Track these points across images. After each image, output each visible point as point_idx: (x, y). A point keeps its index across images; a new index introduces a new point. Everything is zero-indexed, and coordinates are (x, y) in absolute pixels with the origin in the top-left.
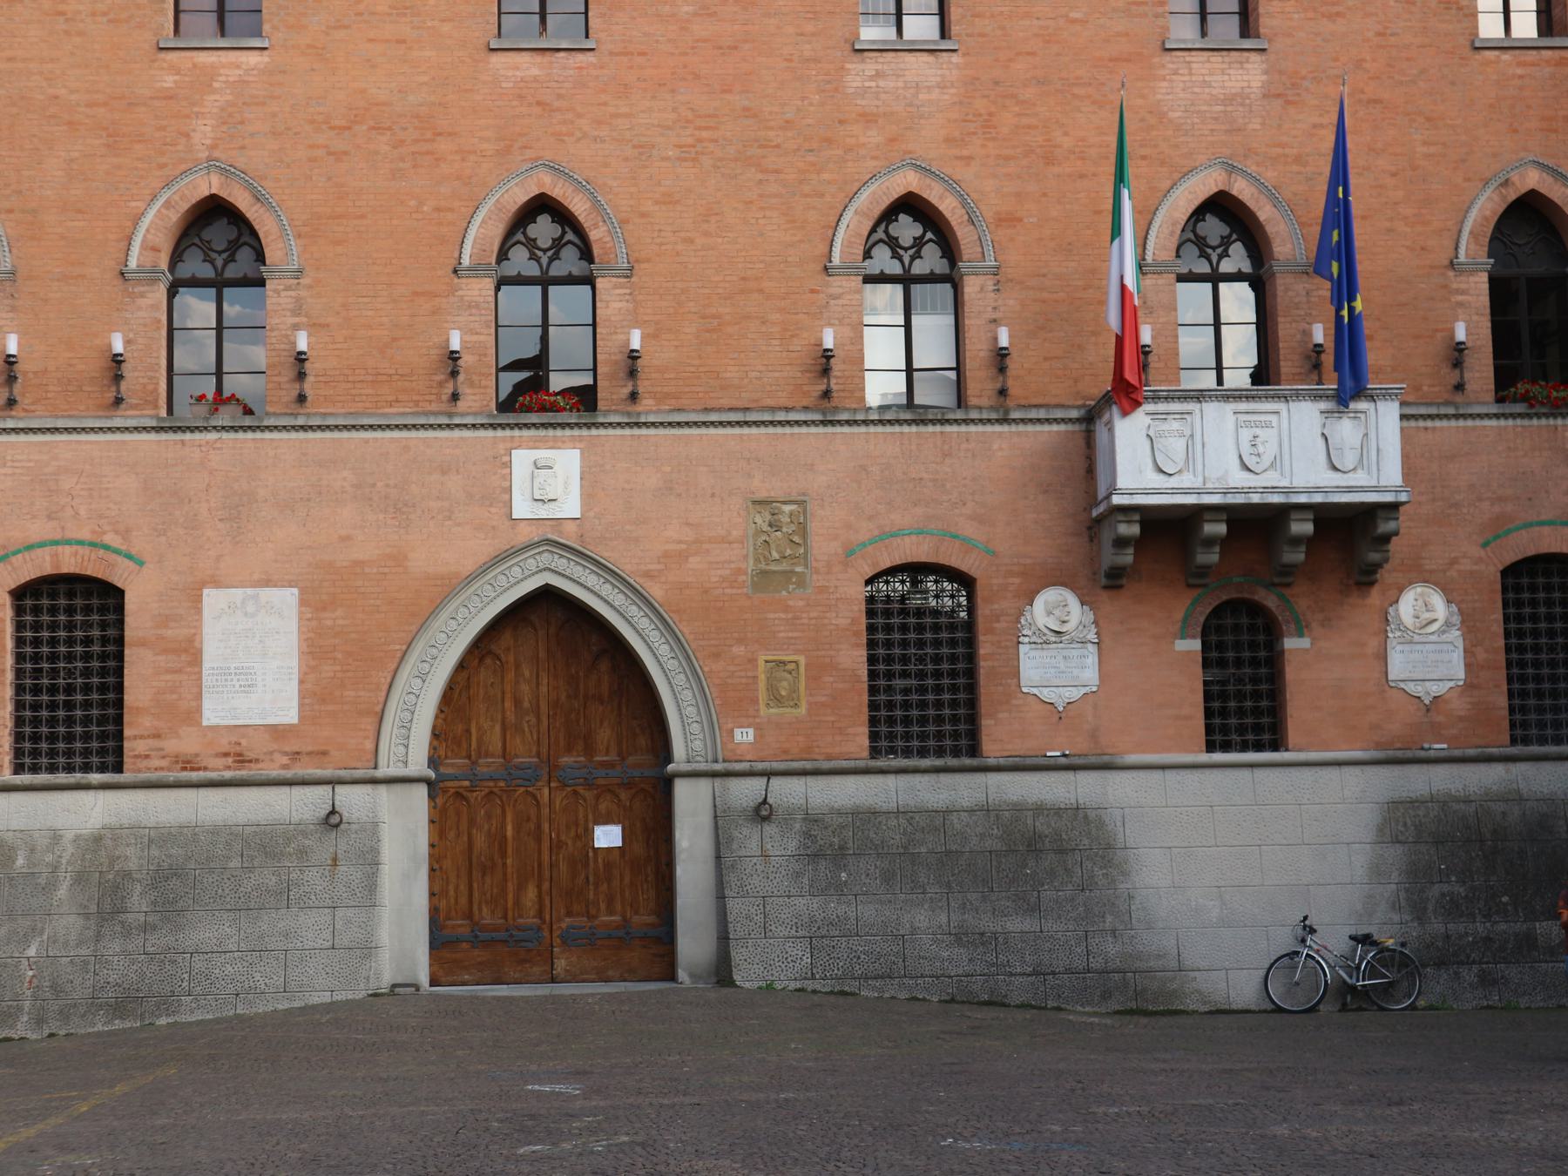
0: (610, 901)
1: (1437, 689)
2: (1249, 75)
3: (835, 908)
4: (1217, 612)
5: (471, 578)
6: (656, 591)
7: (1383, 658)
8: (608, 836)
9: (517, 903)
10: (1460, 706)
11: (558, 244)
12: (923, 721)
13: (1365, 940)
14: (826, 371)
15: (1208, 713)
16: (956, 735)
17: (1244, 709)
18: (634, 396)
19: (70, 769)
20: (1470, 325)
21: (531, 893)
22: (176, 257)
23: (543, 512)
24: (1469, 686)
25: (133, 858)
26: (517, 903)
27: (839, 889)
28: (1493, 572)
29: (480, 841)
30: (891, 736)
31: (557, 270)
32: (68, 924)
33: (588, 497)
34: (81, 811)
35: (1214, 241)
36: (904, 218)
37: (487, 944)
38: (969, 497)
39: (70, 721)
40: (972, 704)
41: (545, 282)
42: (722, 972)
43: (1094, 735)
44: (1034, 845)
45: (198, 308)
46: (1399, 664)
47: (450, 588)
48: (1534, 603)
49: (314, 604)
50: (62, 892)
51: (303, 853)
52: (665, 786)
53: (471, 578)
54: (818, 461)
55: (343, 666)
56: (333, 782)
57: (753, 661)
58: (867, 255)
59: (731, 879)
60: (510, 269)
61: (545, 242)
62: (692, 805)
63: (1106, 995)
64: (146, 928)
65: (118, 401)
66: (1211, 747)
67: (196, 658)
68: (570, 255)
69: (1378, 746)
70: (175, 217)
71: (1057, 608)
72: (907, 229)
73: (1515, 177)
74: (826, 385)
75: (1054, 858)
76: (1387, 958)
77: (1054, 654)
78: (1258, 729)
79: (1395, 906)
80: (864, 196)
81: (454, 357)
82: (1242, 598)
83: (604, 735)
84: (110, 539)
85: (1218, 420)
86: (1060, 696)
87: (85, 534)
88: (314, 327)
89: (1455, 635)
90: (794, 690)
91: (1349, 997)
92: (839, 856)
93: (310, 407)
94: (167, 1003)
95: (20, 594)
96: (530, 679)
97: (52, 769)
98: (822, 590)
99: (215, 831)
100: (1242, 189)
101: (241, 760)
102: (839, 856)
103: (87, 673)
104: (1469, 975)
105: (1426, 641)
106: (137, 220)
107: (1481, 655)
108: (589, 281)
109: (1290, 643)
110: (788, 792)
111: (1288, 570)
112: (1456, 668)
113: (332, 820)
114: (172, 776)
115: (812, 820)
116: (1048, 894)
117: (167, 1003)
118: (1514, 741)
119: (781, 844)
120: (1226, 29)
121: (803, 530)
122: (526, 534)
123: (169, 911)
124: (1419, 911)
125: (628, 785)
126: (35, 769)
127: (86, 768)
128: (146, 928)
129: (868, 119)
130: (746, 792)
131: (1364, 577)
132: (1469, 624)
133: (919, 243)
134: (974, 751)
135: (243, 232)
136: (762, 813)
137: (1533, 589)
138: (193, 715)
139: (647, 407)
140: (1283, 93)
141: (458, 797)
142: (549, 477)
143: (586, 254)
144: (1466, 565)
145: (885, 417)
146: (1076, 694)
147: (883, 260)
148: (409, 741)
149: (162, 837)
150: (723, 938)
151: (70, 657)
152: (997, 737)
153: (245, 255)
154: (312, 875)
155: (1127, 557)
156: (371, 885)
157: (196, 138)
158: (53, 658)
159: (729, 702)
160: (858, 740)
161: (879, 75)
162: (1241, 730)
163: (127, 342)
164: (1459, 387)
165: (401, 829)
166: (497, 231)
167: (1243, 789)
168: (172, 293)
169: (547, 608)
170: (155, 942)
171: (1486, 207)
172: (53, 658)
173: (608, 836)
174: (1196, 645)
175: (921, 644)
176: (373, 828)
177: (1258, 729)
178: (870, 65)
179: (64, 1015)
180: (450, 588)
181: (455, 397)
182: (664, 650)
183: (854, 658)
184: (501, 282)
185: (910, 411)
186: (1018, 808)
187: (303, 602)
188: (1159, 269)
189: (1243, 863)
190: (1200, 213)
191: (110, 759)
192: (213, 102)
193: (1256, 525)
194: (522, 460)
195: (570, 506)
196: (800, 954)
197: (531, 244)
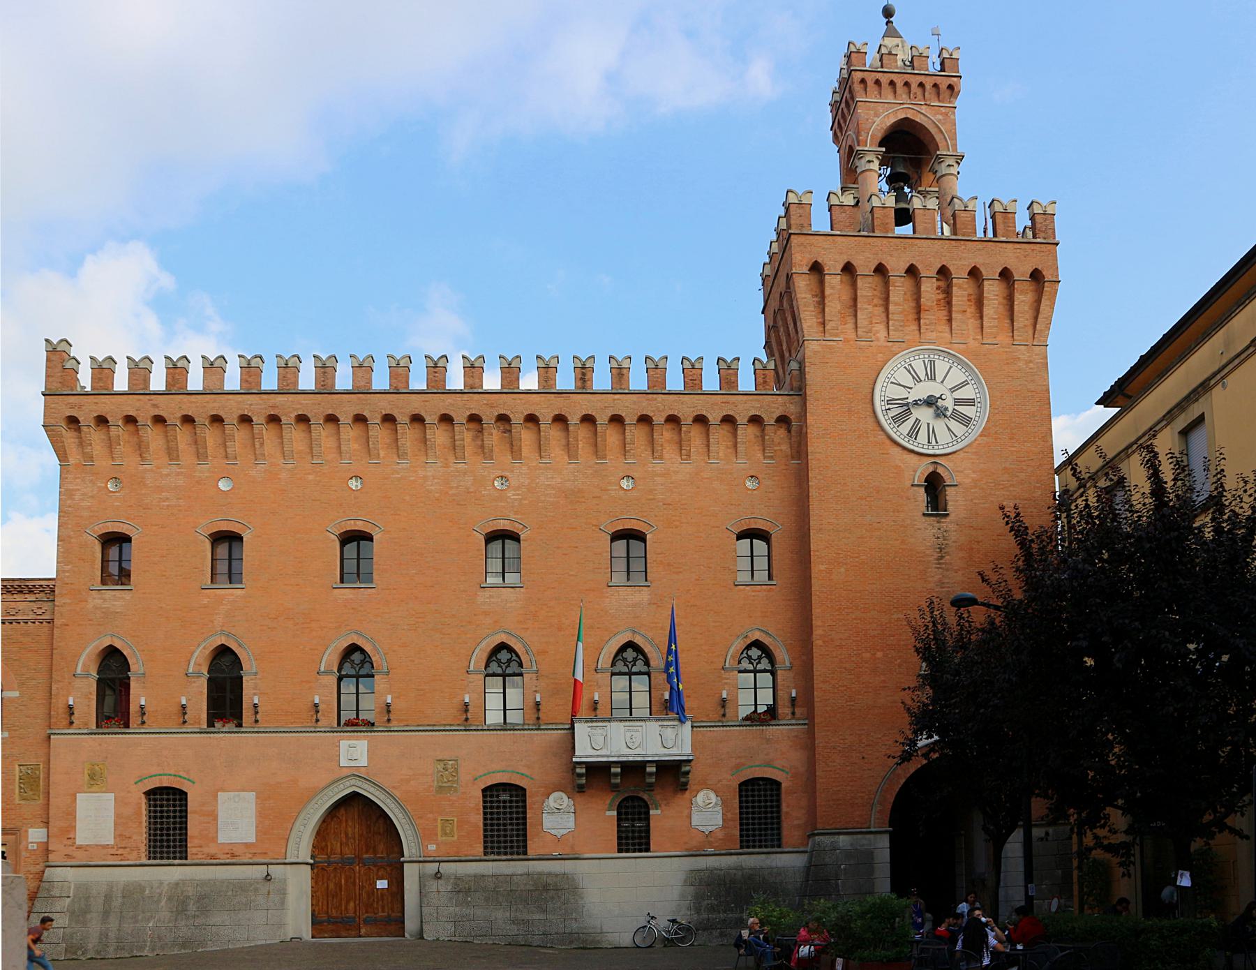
0: (383, 908)
1: (711, 829)
2: (643, 596)
3: (465, 911)
4: (625, 799)
6: (397, 793)
7: (690, 817)
8: (382, 884)
9: (346, 909)
10: (720, 835)
12: (505, 842)
13: (674, 921)
14: (466, 711)
15: (619, 838)
16: (518, 847)
17: (634, 836)
18: (389, 720)
19: (168, 858)
21: (352, 905)
23: (353, 764)
24: (724, 827)
25: (190, 891)
26: (346, 909)
27: (468, 904)
28: (736, 785)
29: (331, 886)
30: (748, 841)
31: (634, 669)
32: (165, 914)
33: (370, 759)
34: (170, 874)
35: (755, 657)
36: (630, 650)
37: (334, 923)
38: (521, 761)
39: (168, 841)
40: (525, 835)
42: (420, 935)
43: (572, 847)
44: (546, 888)
45: (348, 687)
46: (696, 820)
48: (753, 796)
50: (163, 903)
51: (256, 890)
52: (401, 866)
54: (463, 745)
55: (274, 821)
56: (267, 864)
57: (436, 820)
58: (740, 662)
59: (425, 900)
60: (616, 669)
61: (755, 657)
62: (411, 874)
63: (571, 942)
64: (194, 916)
65: (185, 722)
66: (620, 851)
67: (216, 818)
68: (514, 665)
69: (687, 850)
71: (559, 800)
73: (750, 634)
74: (467, 718)
75: (552, 893)
76: (682, 927)
77: (556, 817)
78: (640, 844)
79: (689, 909)
80: (484, 643)
81: (316, 706)
82: (633, 796)
83: (381, 846)
84: (181, 774)
85: (617, 729)
86: (559, 833)
87: (172, 772)
88: (261, 694)
89: (719, 808)
90: (452, 830)
91: (668, 942)
92: (468, 891)
93: (260, 724)
94: (202, 943)
96: (351, 826)
97: (162, 858)
98: (464, 793)
99: (222, 881)
101: (233, 856)
102: (468, 891)
103: (174, 823)
104: (716, 933)
105: (708, 811)
106: (192, 654)
107: (729, 815)
108: (521, 675)
109: (652, 812)
110: (445, 868)
111: (651, 785)
112: (719, 821)
113: (268, 878)
114: (206, 861)
115: (458, 878)
116: (550, 906)
117: (202, 943)
118: (742, 847)
119: (444, 887)
121: (456, 770)
122: (346, 772)
123: (204, 910)
124: (698, 911)
125: (390, 865)
126: (155, 858)
127: (175, 858)
128: (194, 916)
129: (486, 613)
131: (683, 788)
132: (725, 804)
133: (760, 658)
134: (525, 853)
135: (366, 659)
136: (438, 876)
137: (753, 790)
138: (215, 839)
139: (394, 725)
141: (324, 868)
142: (355, 751)
144: (725, 782)
146: (565, 832)
147: (745, 665)
148: (302, 844)
149: (202, 883)
151: (168, 817)
152: (533, 847)
153: (367, 665)
154: (259, 898)
155: (583, 781)
157: (216, 623)
158: (162, 817)
159: (427, 835)
160: (479, 849)
161: (491, 597)
162: (634, 844)
163: (188, 700)
164: (724, 715)
166: (485, 656)
167: (635, 866)
168: (340, 679)
169: (353, 799)
170: (198, 921)
172: (162, 817)
173: (382, 884)
174: (615, 813)
175: (505, 813)
176: (284, 881)
177: (640, 844)
178: (487, 593)
179: (162, 948)
181: (317, 721)
182: (400, 815)
183: (478, 819)
184: (613, 674)
185: (505, 726)
186: (540, 874)
187: (257, 798)
188: (603, 671)
189: (630, 893)
190: (623, 649)
191: (521, 850)
193: (633, 769)
194: (344, 744)
195: (363, 762)
196: (450, 928)
197: (499, 661)
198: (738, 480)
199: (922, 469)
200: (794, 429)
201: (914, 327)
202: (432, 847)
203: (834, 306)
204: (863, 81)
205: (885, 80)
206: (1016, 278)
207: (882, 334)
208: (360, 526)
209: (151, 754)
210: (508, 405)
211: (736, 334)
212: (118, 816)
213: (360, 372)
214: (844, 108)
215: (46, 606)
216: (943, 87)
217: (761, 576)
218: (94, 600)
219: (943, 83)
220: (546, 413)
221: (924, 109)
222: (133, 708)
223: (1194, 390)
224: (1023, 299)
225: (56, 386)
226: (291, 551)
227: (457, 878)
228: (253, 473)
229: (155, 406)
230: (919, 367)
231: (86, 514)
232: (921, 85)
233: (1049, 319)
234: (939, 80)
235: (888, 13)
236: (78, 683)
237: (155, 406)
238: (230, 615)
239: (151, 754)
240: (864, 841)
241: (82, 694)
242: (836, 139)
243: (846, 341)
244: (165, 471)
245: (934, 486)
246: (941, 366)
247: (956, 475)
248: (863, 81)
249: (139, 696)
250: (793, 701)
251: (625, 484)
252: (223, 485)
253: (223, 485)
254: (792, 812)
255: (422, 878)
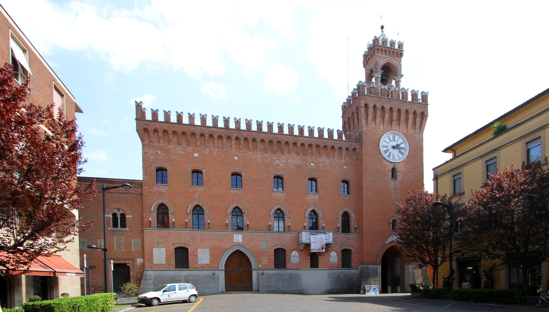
2: (317, 197)
5: (229, 248)
6: (251, 250)
10: (337, 264)
11: (200, 210)
20: (339, 225)
22: (193, 211)
24: (338, 262)
41: (198, 214)
46: (331, 260)
47: (227, 250)
49: (211, 251)
53: (229, 248)
62: (254, 273)
70: (193, 206)
71: (295, 253)
72: (278, 212)
74: (270, 228)
77: (294, 257)
88: (210, 220)
95: (176, 249)
100: (316, 209)
105: (334, 257)
110: (265, 272)
112: (298, 260)
113: (214, 274)
120: (314, 191)
122: (236, 244)
129: (275, 199)
130: (261, 272)
132: (338, 255)
136: (263, 274)
138: (197, 263)
140: (320, 199)
142: (238, 238)
143: (242, 213)
145: (276, 232)
147: (234, 213)
148: (222, 266)
150: (258, 287)
152: (288, 266)
153: (201, 211)
156: (219, 281)
165: (222, 276)
166: (232, 210)
169: (238, 251)
171: (341, 213)
180: (227, 250)
183: (273, 258)
190: (277, 210)
192: (197, 193)
194: (235, 236)
195: (241, 241)
198: (333, 167)
199: (391, 166)
200: (357, 152)
201: (390, 126)
202: (260, 266)
203: (370, 118)
204: (378, 49)
205: (384, 49)
206: (413, 113)
207: (382, 127)
208: (238, 171)
209: (178, 236)
210: (280, 138)
211: (333, 122)
212: (167, 255)
213: (238, 124)
214: (368, 58)
215: (139, 189)
216: (399, 53)
217: (346, 193)
218: (156, 189)
219: (399, 52)
220: (291, 141)
221: (394, 60)
222: (170, 222)
223: (524, 135)
224: (418, 120)
225: (139, 117)
226: (217, 176)
227: (268, 275)
228: (205, 152)
229: (173, 127)
230: (391, 137)
231: (151, 160)
232: (393, 52)
233: (424, 126)
234: (398, 51)
235: (382, 27)
236: (152, 214)
237: (173, 127)
238: (199, 195)
239: (178, 236)
240: (375, 266)
241: (152, 218)
242: (364, 66)
243: (373, 128)
244: (177, 149)
245: (394, 170)
246: (397, 137)
247: (399, 168)
248: (378, 49)
249: (172, 219)
250: (356, 228)
251: (312, 164)
252: (196, 155)
253: (196, 155)
254: (355, 258)
255: (258, 274)
